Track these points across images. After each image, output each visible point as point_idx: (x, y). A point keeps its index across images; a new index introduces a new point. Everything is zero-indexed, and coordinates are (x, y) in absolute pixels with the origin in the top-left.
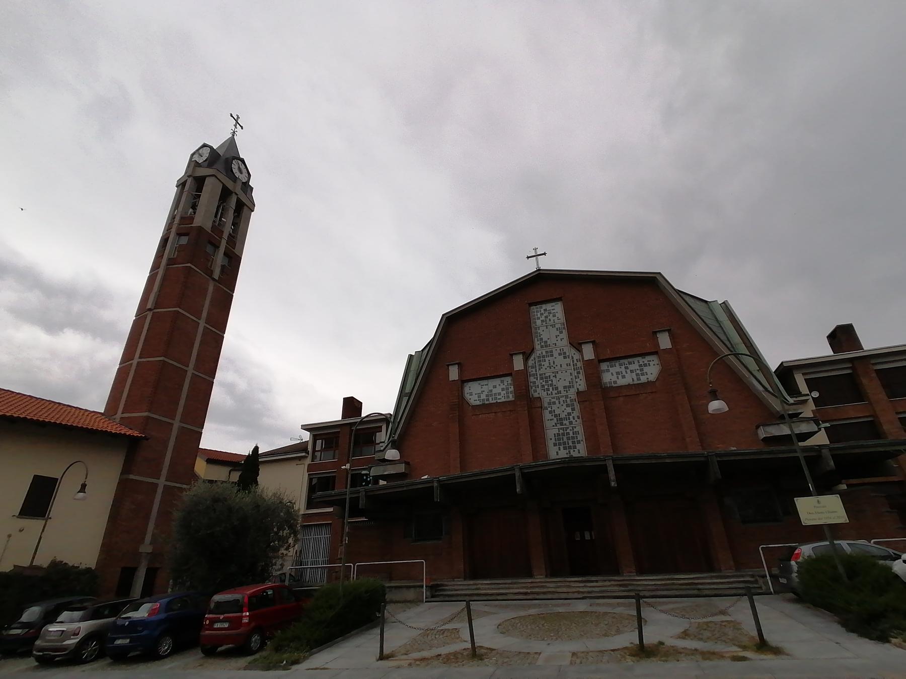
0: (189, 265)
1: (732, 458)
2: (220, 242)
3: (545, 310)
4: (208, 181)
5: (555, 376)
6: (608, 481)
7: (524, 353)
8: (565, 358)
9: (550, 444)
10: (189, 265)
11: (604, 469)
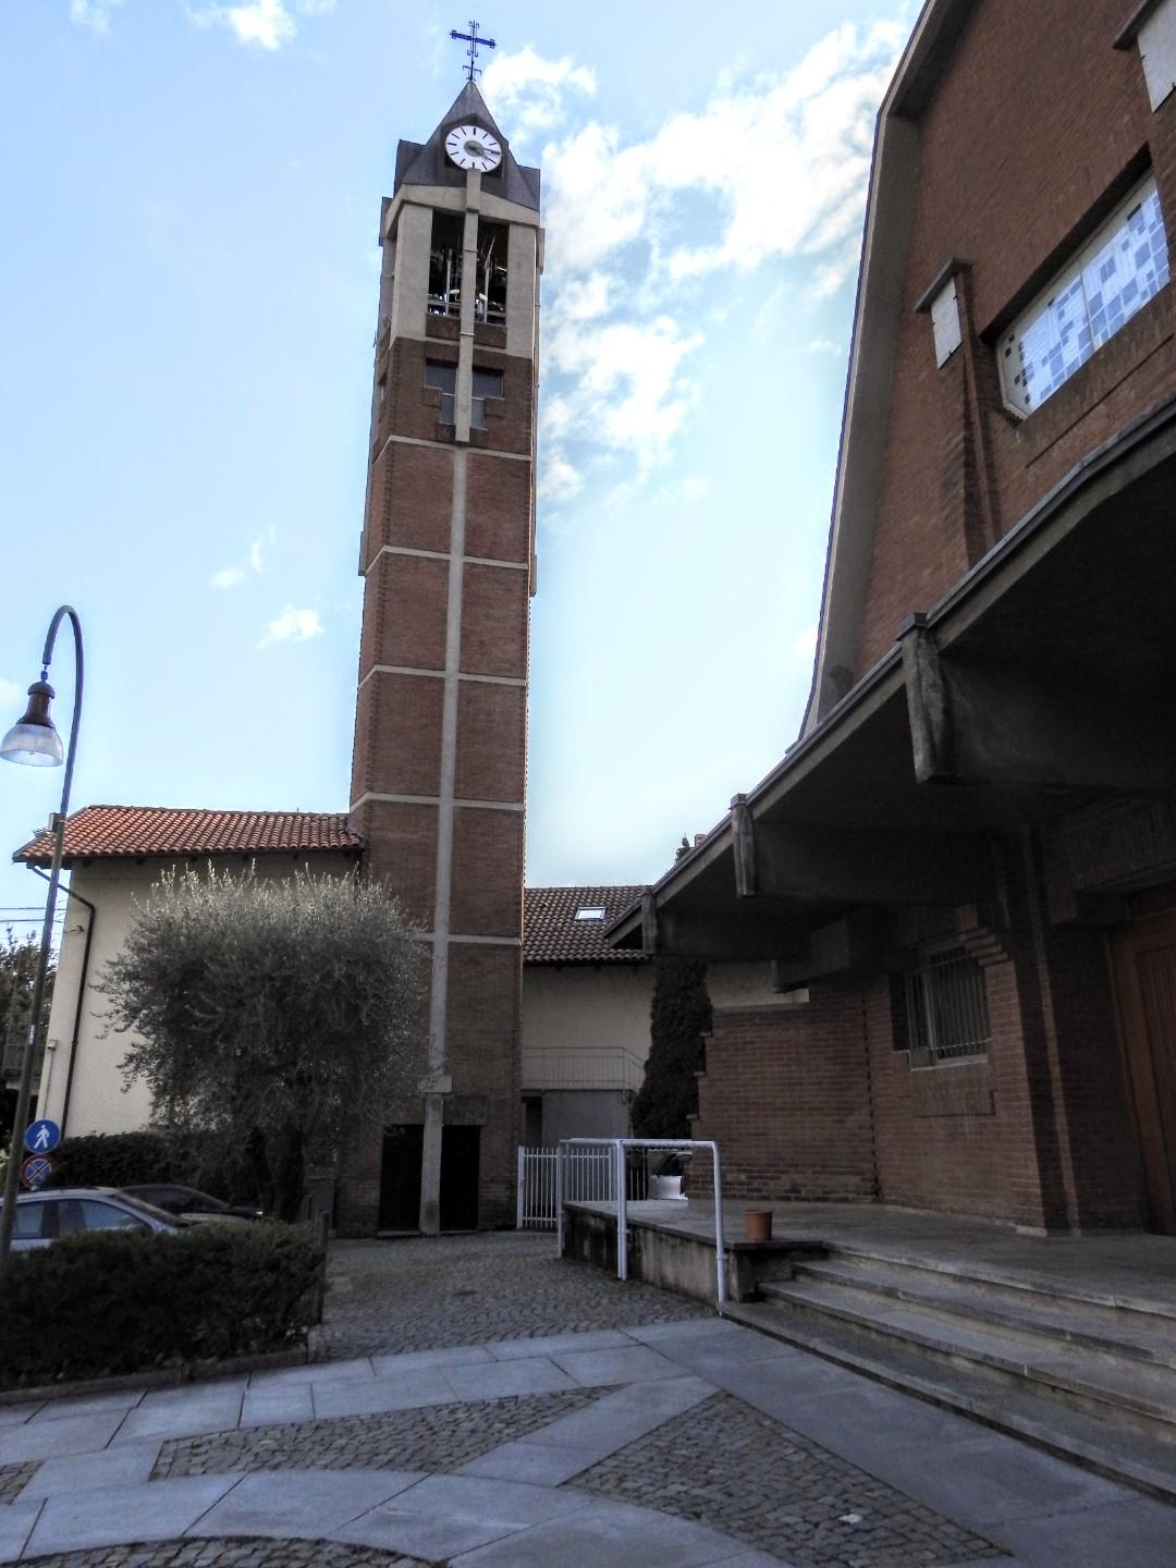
2: (457, 351)
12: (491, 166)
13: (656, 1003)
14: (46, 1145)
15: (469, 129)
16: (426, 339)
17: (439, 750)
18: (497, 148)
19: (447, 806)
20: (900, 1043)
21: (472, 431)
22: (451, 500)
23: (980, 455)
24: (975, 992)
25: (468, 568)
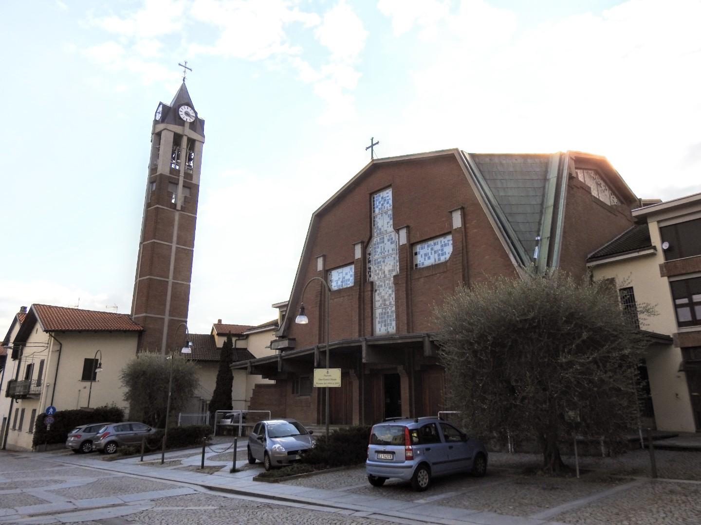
0: (157, 206)
1: (264, 362)
2: (178, 179)
3: (382, 198)
4: (163, 134)
5: (384, 262)
6: (361, 358)
7: (362, 243)
8: (392, 243)
9: (377, 320)
10: (157, 206)
11: (360, 347)
12: (192, 120)
13: (219, 375)
14: (52, 413)
15: (186, 107)
16: (169, 175)
17: (166, 302)
18: (194, 115)
19: (167, 318)
20: (293, 393)
21: (182, 206)
22: (174, 227)
23: (323, 293)
24: (321, 405)
25: (177, 248)
